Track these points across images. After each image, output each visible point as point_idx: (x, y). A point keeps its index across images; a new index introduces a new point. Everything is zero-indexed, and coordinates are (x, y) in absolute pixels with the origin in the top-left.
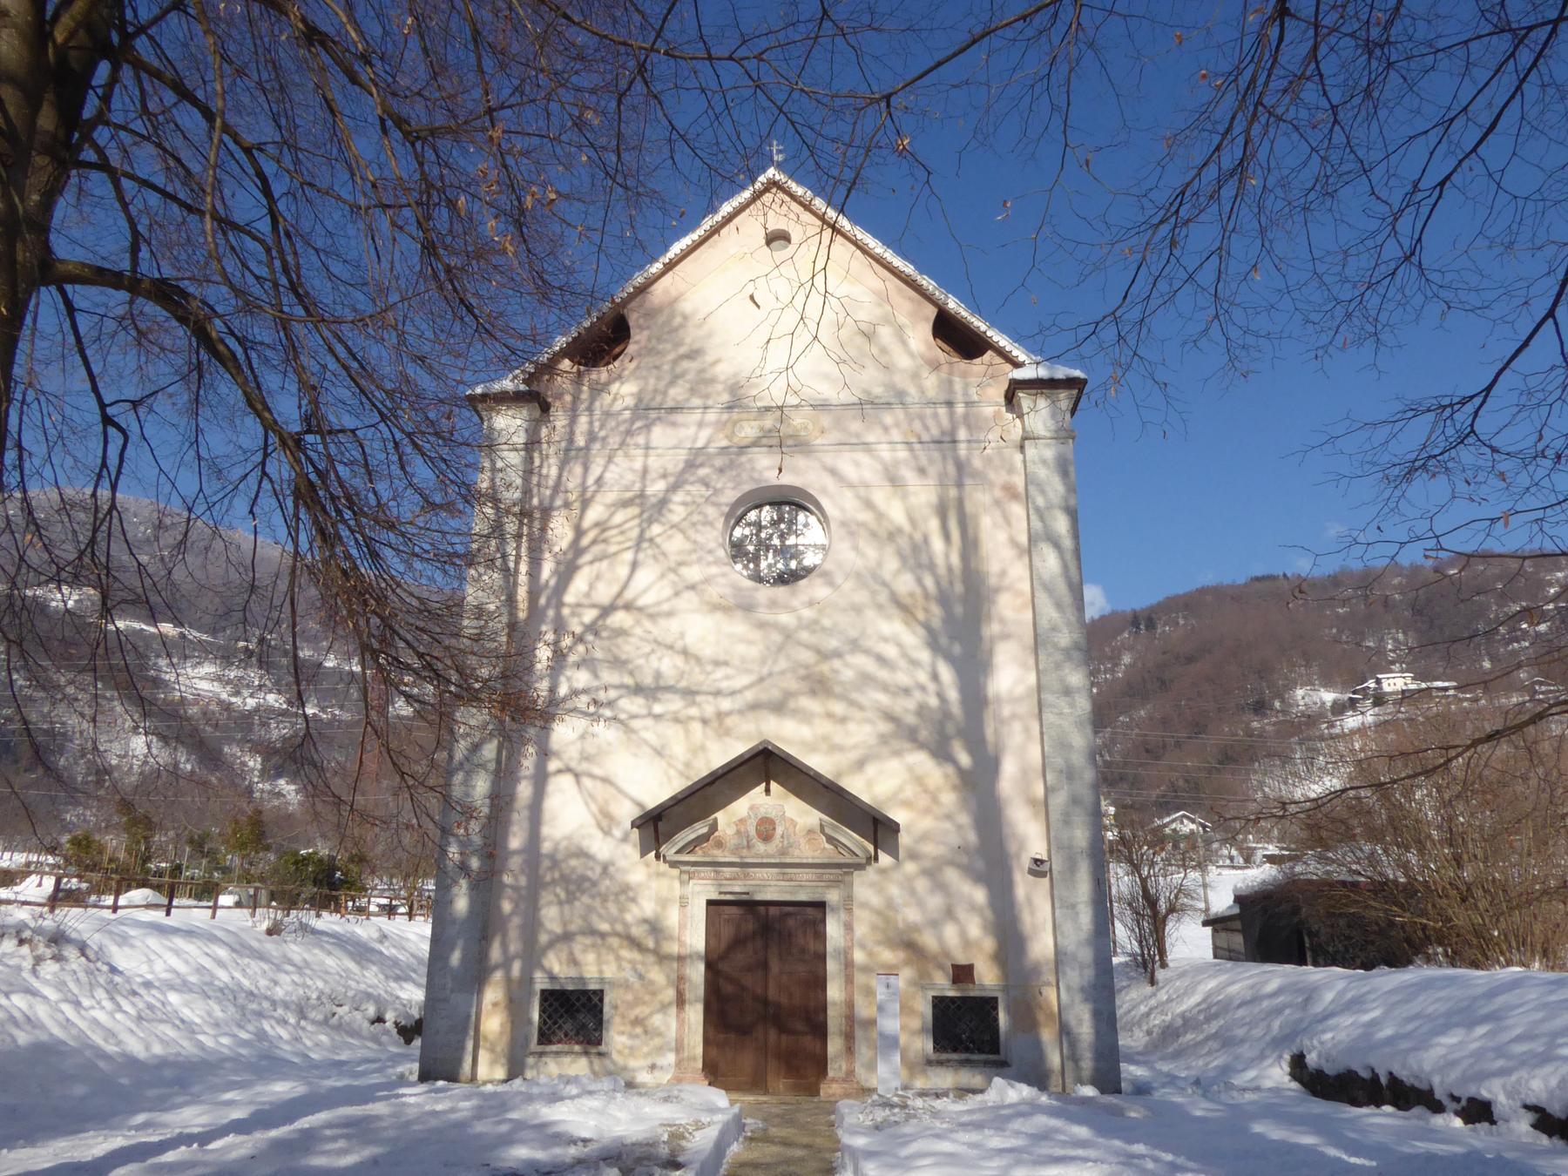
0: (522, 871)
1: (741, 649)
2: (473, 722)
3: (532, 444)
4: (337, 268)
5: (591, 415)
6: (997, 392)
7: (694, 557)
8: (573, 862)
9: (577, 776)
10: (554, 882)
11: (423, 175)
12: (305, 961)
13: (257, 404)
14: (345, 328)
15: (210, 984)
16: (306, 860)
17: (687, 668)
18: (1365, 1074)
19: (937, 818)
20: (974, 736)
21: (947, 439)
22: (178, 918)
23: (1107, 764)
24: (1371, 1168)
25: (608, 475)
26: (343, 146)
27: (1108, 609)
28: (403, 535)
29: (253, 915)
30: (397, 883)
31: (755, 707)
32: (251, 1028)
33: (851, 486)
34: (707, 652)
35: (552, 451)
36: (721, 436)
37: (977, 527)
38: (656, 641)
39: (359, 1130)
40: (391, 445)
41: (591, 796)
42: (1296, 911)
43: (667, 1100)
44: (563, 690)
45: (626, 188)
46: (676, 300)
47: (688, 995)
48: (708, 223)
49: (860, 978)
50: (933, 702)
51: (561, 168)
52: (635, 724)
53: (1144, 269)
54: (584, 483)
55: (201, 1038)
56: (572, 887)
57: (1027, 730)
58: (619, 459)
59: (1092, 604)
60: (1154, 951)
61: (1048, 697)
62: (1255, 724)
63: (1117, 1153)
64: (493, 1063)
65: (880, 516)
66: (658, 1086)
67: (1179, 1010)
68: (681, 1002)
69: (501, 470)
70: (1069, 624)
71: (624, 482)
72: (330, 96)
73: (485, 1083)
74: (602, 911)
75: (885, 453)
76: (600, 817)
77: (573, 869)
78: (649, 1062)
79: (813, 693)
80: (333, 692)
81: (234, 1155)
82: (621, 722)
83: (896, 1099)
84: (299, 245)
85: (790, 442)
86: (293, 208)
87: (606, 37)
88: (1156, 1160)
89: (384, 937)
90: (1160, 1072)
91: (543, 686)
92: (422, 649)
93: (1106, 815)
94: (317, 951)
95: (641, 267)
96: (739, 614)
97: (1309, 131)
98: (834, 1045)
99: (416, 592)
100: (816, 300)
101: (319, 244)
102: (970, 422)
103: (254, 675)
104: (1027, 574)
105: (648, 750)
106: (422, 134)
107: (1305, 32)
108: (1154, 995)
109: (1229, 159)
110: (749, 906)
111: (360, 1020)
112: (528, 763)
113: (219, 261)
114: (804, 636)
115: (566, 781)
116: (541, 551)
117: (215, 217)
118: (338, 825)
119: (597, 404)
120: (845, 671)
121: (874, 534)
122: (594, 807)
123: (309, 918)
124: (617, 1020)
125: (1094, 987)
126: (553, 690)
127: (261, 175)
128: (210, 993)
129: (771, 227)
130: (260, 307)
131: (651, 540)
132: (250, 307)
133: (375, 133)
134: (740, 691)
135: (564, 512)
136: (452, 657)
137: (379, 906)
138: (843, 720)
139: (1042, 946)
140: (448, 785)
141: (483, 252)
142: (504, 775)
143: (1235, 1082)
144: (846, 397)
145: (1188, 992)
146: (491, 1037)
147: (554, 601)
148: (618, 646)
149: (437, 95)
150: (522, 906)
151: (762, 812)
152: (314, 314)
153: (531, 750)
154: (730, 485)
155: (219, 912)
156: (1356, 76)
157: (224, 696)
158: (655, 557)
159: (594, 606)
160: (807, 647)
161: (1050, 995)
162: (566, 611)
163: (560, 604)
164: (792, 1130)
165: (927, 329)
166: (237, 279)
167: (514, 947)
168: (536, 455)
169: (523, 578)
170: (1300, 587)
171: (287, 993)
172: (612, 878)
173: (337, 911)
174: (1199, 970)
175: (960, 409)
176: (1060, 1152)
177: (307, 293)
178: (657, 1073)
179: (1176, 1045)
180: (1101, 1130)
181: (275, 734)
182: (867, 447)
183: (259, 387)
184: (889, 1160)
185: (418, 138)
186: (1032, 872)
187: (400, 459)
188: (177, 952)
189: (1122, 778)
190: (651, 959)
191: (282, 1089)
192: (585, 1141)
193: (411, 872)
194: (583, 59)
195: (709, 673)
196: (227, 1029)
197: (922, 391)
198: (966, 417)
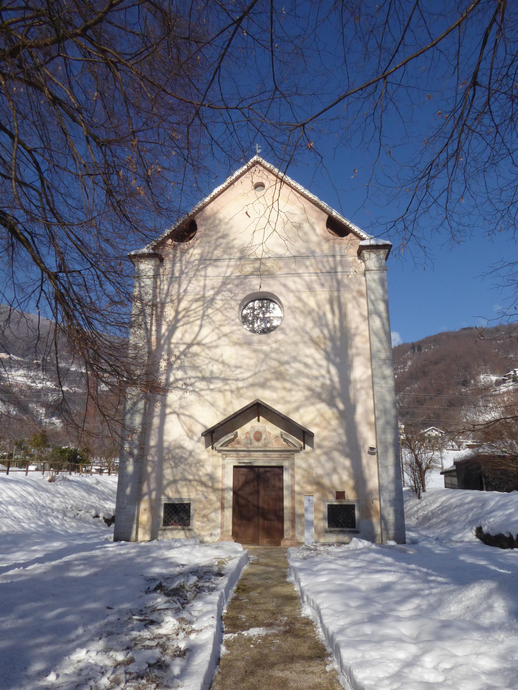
0: (156, 455)
1: (247, 361)
2: (134, 393)
3: (156, 276)
4: (70, 201)
5: (181, 263)
6: (354, 251)
7: (226, 322)
8: (177, 451)
9: (178, 415)
10: (169, 459)
11: (106, 162)
12: (65, 492)
13: (38, 260)
14: (75, 227)
15: (26, 502)
16: (65, 451)
17: (224, 369)
18: (507, 535)
19: (329, 431)
20: (345, 396)
21: (333, 271)
22: (12, 475)
23: (401, 407)
24: (509, 574)
25: (189, 288)
26: (70, 149)
27: (401, 342)
28: (102, 315)
29: (43, 474)
30: (103, 460)
31: (253, 385)
32: (43, 520)
33: (292, 291)
34: (232, 362)
35: (165, 278)
36: (237, 271)
37: (346, 308)
38: (211, 358)
39: (89, 561)
40: (95, 277)
41: (185, 423)
42: (479, 468)
43: (217, 548)
44: (172, 379)
45: (193, 165)
46: (216, 213)
47: (226, 505)
48: (229, 180)
49: (297, 497)
50: (328, 382)
51: (165, 157)
52: (203, 393)
53: (415, 198)
54: (179, 292)
55: (23, 524)
56: (177, 461)
57: (367, 394)
58: (194, 281)
59: (394, 340)
60: (420, 485)
61: (376, 380)
62: (463, 390)
63: (403, 568)
64: (144, 534)
65: (305, 304)
66: (214, 542)
67: (430, 509)
68: (223, 508)
69: (143, 287)
70: (385, 349)
71: (196, 291)
72: (64, 127)
73: (141, 542)
74: (190, 471)
75: (307, 277)
76: (188, 432)
77: (177, 454)
78: (210, 532)
79: (277, 379)
80: (74, 381)
81: (38, 572)
82: (197, 392)
83: (312, 547)
84: (53, 191)
85: (266, 273)
86: (50, 176)
87: (182, 99)
88: (419, 571)
89: (98, 482)
90: (422, 535)
91: (163, 378)
92: (111, 363)
93: (400, 428)
94: (70, 489)
95: (201, 199)
96: (246, 346)
97: (486, 136)
98: (287, 525)
99: (108, 338)
100: (274, 214)
101: (62, 191)
102: (342, 263)
103: (40, 374)
104: (367, 328)
105: (208, 404)
106: (105, 143)
107: (484, 93)
108: (420, 503)
109: (452, 148)
110: (251, 468)
111: (89, 516)
112: (157, 410)
113: (19, 200)
114: (273, 355)
115: (174, 417)
116: (161, 321)
117: (17, 180)
118: (78, 437)
119: (184, 258)
120: (291, 369)
121: (302, 312)
122: (186, 428)
123: (66, 474)
124: (196, 515)
125: (395, 500)
126: (167, 379)
127: (35, 162)
128: (26, 506)
129: (255, 181)
130: (37, 219)
131: (208, 316)
132: (33, 219)
133: (84, 143)
134: (247, 379)
135: (170, 304)
136: (124, 366)
137: (96, 469)
138: (290, 390)
139: (373, 483)
140: (124, 419)
141: (133, 194)
142: (148, 415)
143: (453, 539)
144: (288, 254)
145: (434, 502)
146: (144, 523)
147: (167, 342)
148: (195, 361)
149: (110, 126)
150: (156, 469)
151: (256, 429)
152: (62, 223)
153: (159, 404)
154: (241, 292)
155: (29, 473)
156: (507, 111)
157: (28, 383)
158: (210, 323)
159: (184, 344)
160: (275, 360)
161: (377, 503)
162: (172, 346)
163: (170, 343)
164: (269, 560)
165: (323, 224)
166: (27, 207)
167: (153, 486)
168: (158, 280)
169: (154, 333)
170: (482, 332)
171: (58, 506)
172: (193, 457)
173: (78, 472)
174: (439, 493)
175: (338, 258)
176: (380, 568)
177: (57, 212)
178: (213, 537)
179: (429, 524)
180: (398, 559)
181: (51, 399)
182: (299, 275)
183: (38, 253)
184: (309, 572)
185: (103, 145)
186: (369, 453)
187: (100, 283)
188: (12, 490)
189: (407, 413)
190: (210, 490)
191: (57, 545)
192: (183, 565)
193: (109, 455)
194: (172, 109)
195: (233, 371)
196: (33, 521)
197: (322, 251)
198: (341, 261)
